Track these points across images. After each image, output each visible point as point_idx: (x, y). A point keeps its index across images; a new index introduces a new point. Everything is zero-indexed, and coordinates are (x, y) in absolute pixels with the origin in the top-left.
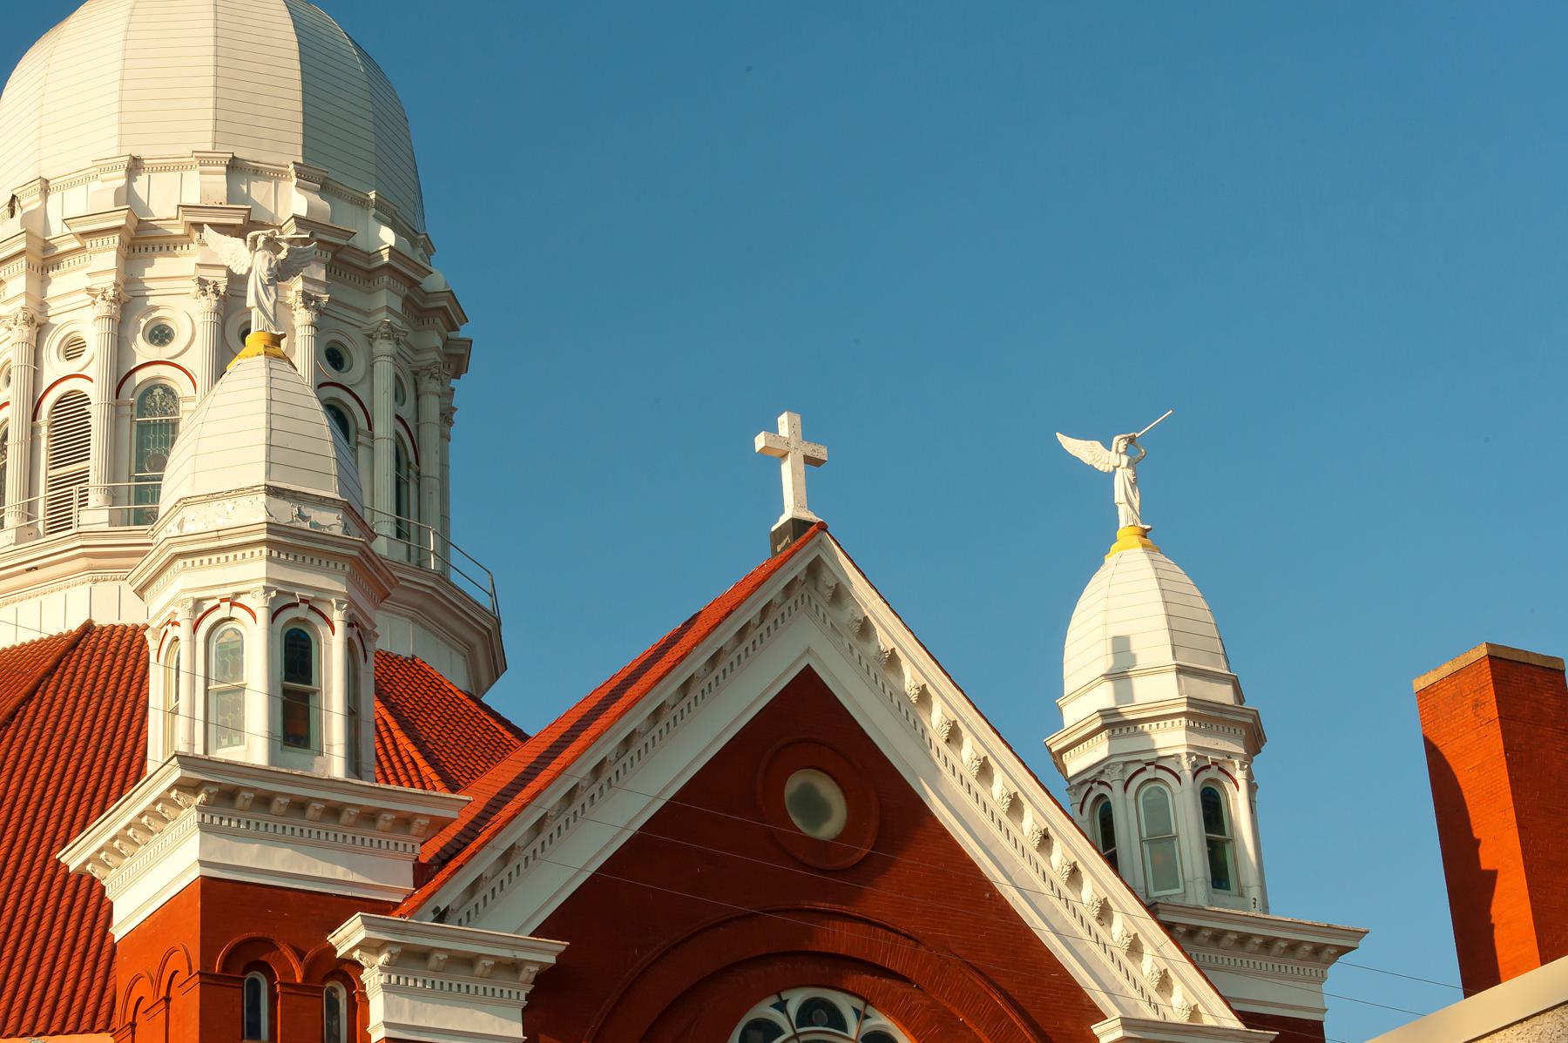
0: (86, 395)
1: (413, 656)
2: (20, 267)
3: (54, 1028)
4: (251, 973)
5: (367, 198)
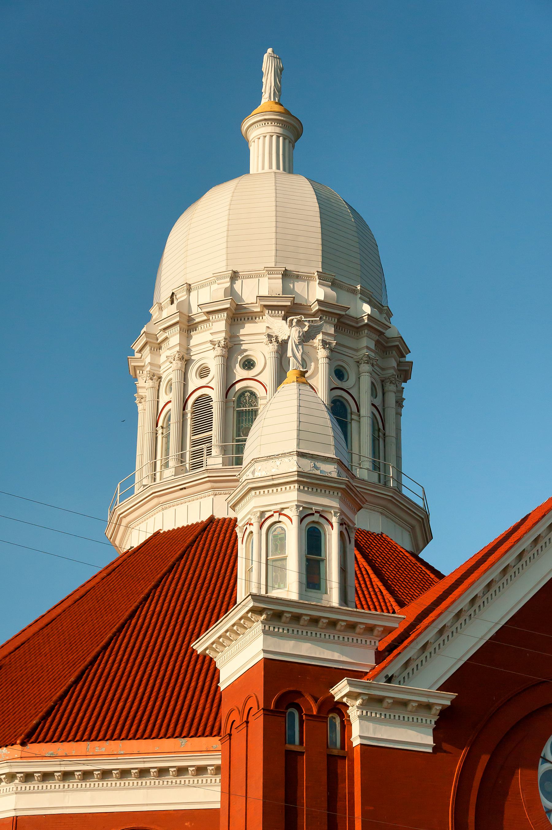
0: (210, 397)
1: (381, 532)
2: (176, 330)
3: (191, 734)
4: (291, 709)
5: (356, 289)
